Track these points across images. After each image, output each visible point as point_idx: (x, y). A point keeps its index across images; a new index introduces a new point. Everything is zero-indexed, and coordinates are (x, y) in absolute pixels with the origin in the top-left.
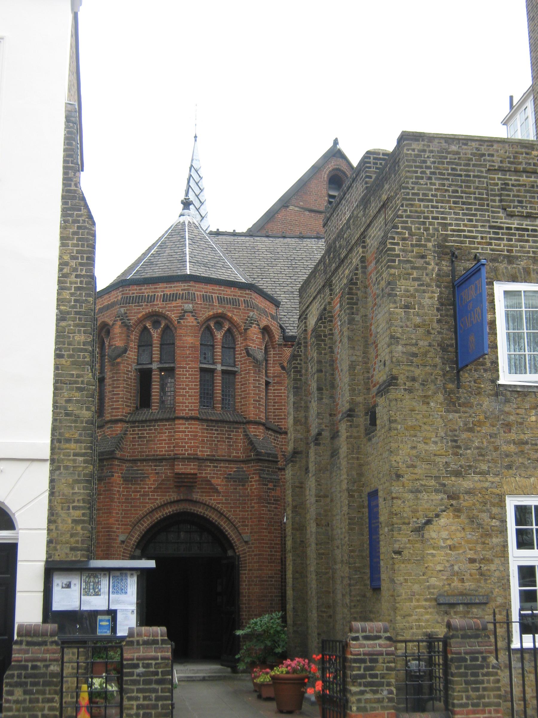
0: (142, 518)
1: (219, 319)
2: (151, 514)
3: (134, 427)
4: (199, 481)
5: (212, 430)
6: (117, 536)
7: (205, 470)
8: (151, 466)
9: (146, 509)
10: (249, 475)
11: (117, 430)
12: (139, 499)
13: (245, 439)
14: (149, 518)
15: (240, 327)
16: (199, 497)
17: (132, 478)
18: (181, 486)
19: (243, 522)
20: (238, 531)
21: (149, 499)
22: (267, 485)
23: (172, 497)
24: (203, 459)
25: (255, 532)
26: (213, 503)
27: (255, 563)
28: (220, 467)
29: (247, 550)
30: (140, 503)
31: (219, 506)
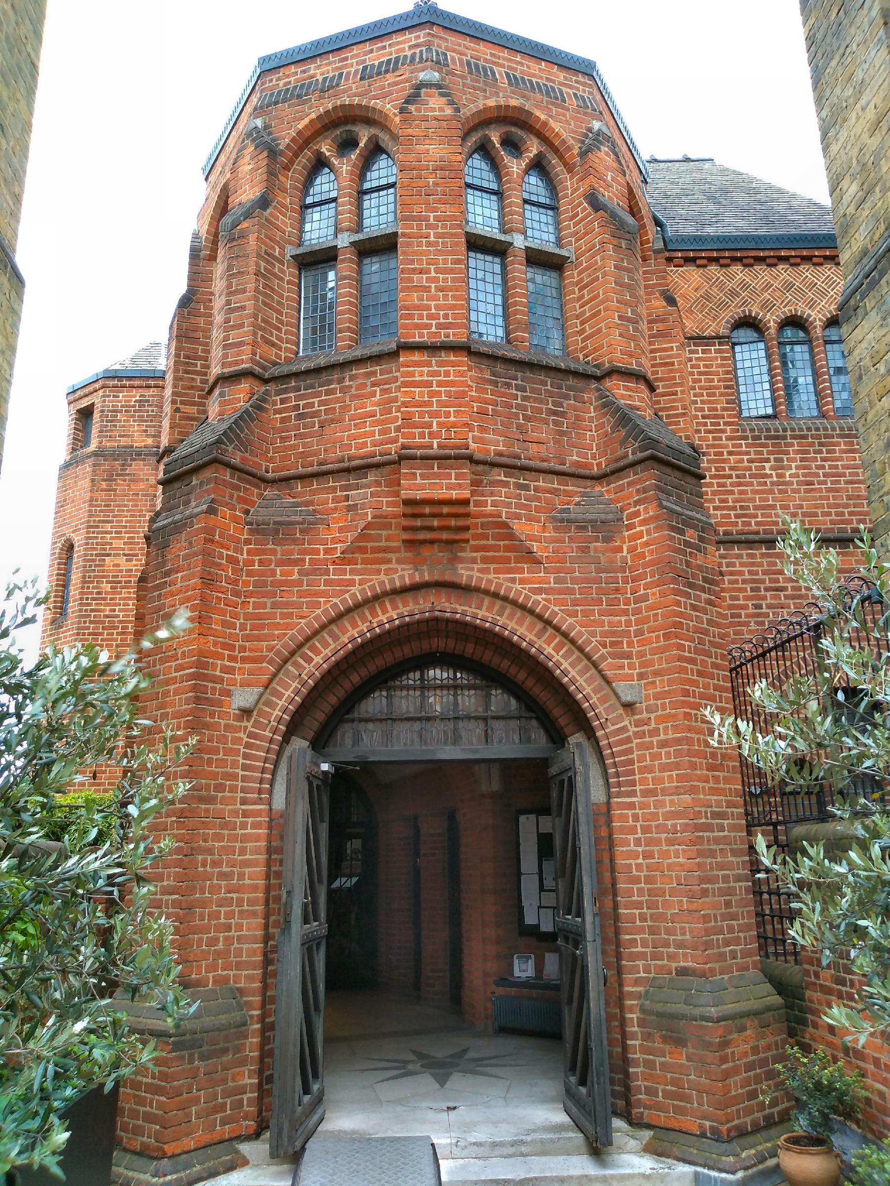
0: (308, 639)
1: (513, 129)
2: (334, 627)
3: (285, 391)
4: (476, 526)
5: (509, 385)
6: (228, 694)
7: (492, 494)
8: (334, 489)
9: (318, 611)
10: (622, 510)
11: (239, 400)
12: (299, 583)
13: (605, 414)
14: (330, 640)
15: (569, 148)
16: (476, 574)
17: (275, 523)
18: (423, 542)
19: (613, 644)
20: (600, 672)
21: (327, 583)
22: (682, 532)
23: (396, 576)
24: (485, 463)
25: (656, 673)
26: (519, 590)
27: (664, 768)
28: (536, 489)
29: (633, 729)
30: (300, 594)
31: (539, 597)
